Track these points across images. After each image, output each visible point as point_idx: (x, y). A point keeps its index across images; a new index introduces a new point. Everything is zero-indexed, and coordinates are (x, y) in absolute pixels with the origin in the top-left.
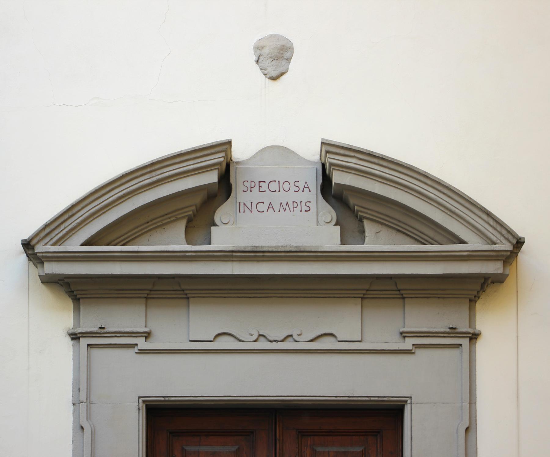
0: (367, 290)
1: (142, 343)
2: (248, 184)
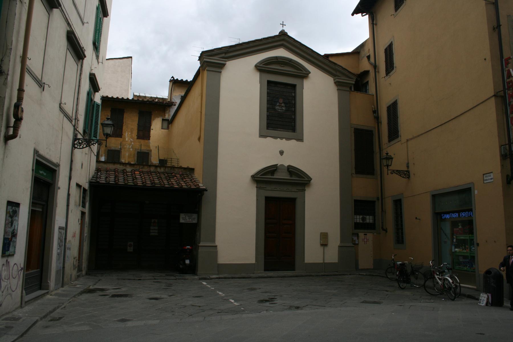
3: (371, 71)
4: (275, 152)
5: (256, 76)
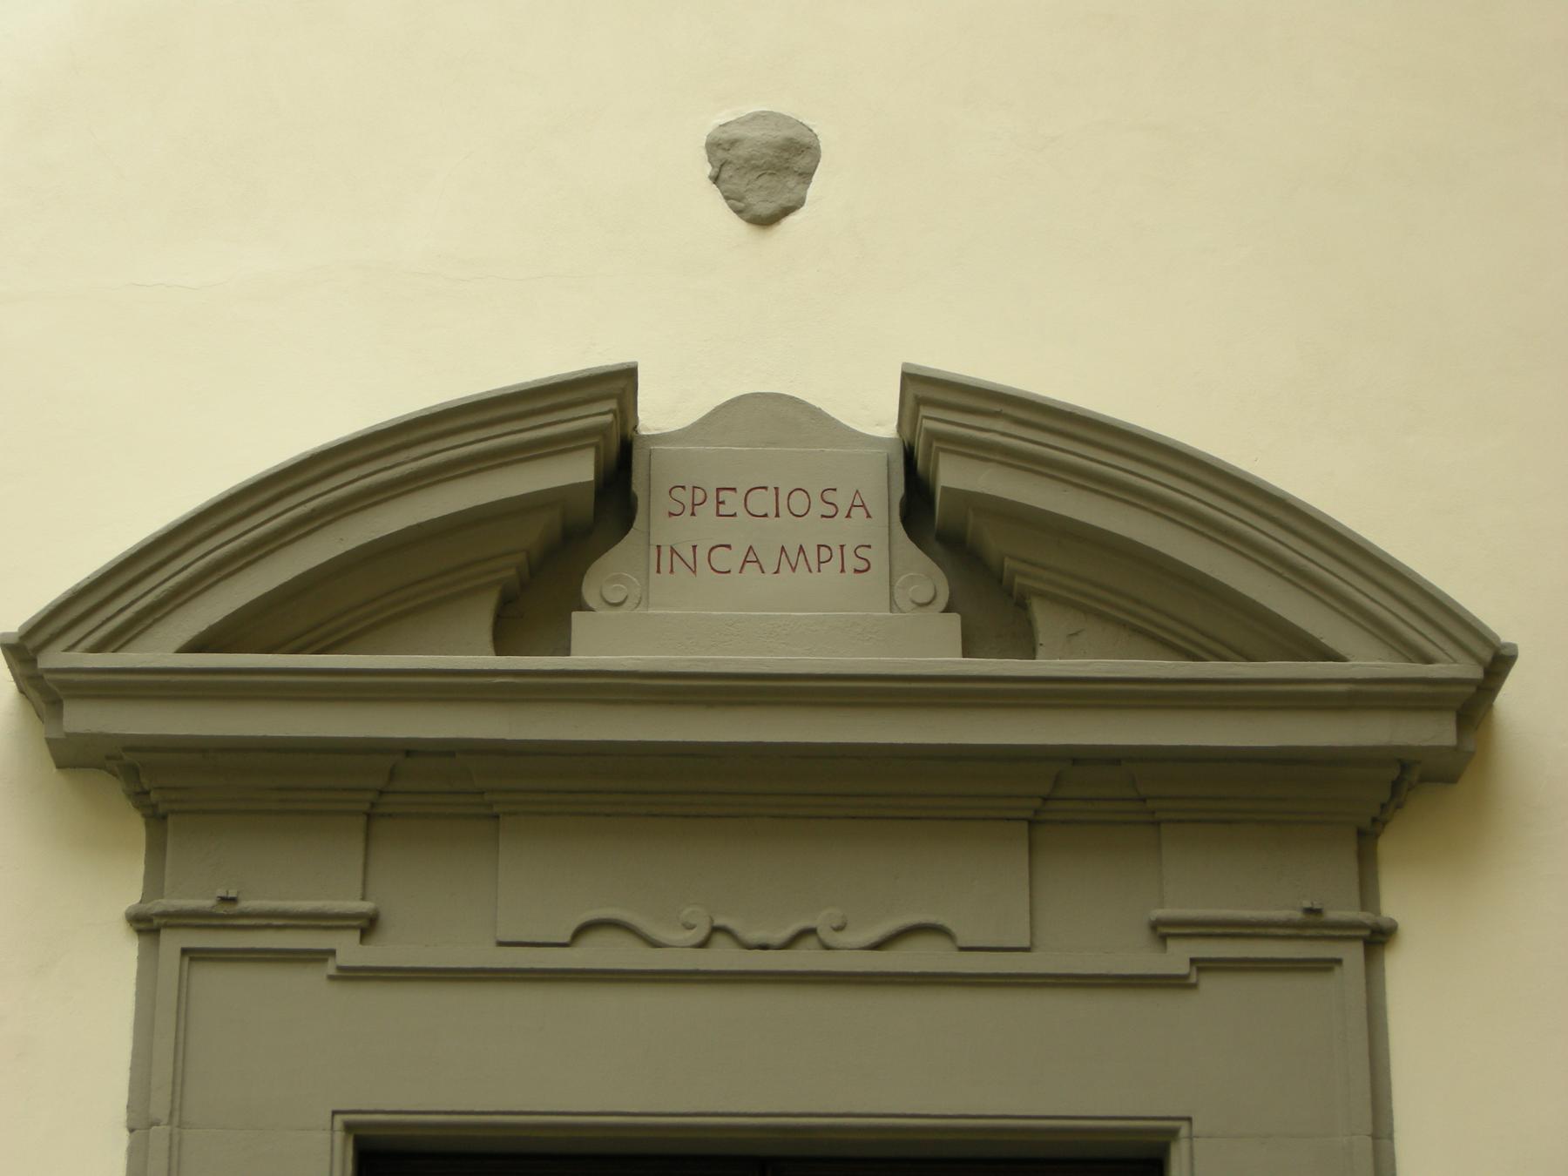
0: (1045, 799)
1: (349, 949)
2: (685, 496)
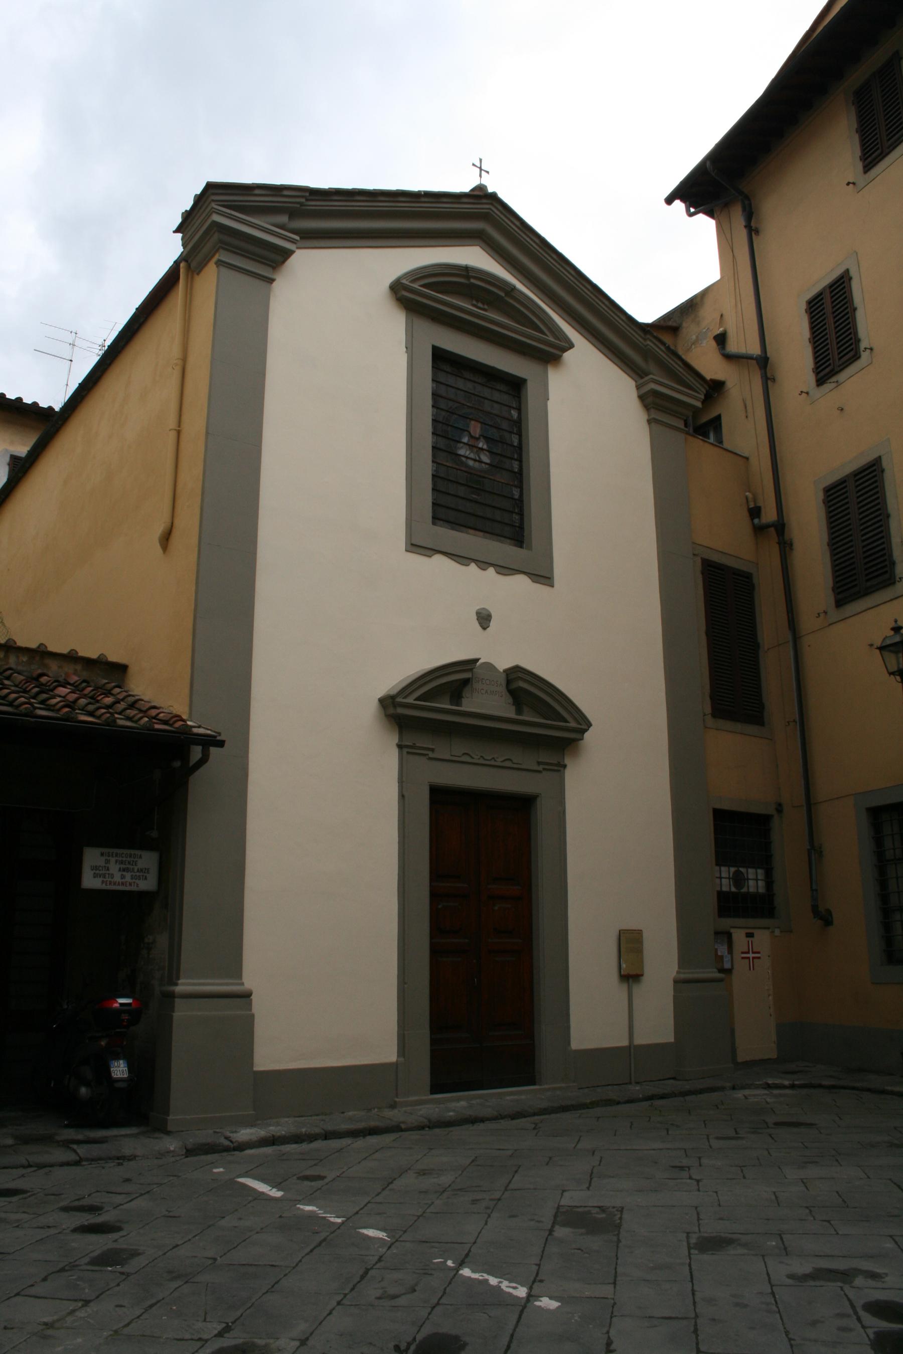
1: (431, 755)
3: (729, 384)
4: (449, 612)
5: (394, 325)
